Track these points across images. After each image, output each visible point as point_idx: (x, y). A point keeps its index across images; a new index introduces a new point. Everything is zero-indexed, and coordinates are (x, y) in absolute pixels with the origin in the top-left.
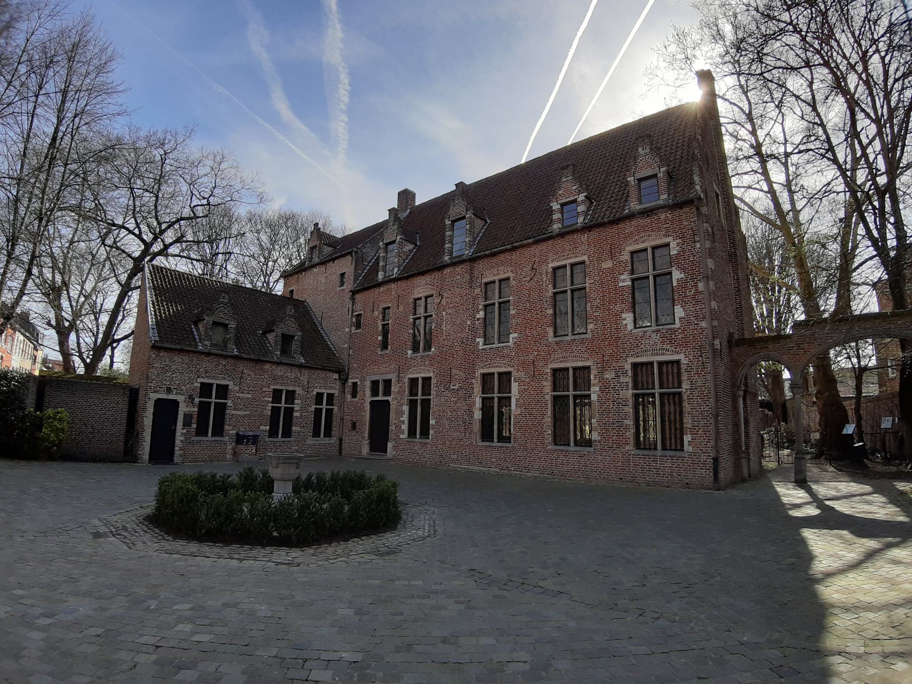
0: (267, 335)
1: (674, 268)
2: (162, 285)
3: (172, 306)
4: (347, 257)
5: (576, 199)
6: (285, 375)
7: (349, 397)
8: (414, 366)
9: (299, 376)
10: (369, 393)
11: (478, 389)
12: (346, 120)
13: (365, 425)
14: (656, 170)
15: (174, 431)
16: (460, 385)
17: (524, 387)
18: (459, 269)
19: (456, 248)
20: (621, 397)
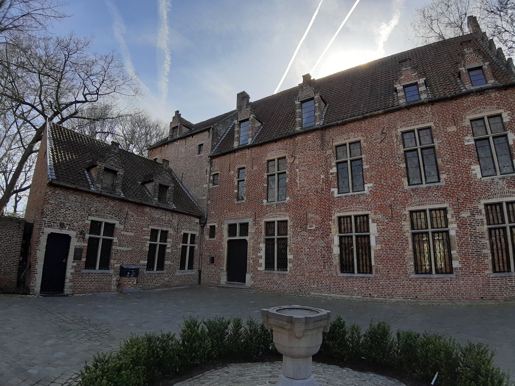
0: (146, 185)
1: (509, 131)
2: (60, 138)
3: (68, 154)
4: (204, 133)
5: (417, 82)
7: (207, 237)
8: (270, 212)
9: (171, 219)
10: (227, 234)
12: (167, 81)
13: (223, 259)
14: (481, 64)
15: (65, 264)
16: (317, 226)
17: (383, 227)
18: (310, 136)
20: (477, 232)
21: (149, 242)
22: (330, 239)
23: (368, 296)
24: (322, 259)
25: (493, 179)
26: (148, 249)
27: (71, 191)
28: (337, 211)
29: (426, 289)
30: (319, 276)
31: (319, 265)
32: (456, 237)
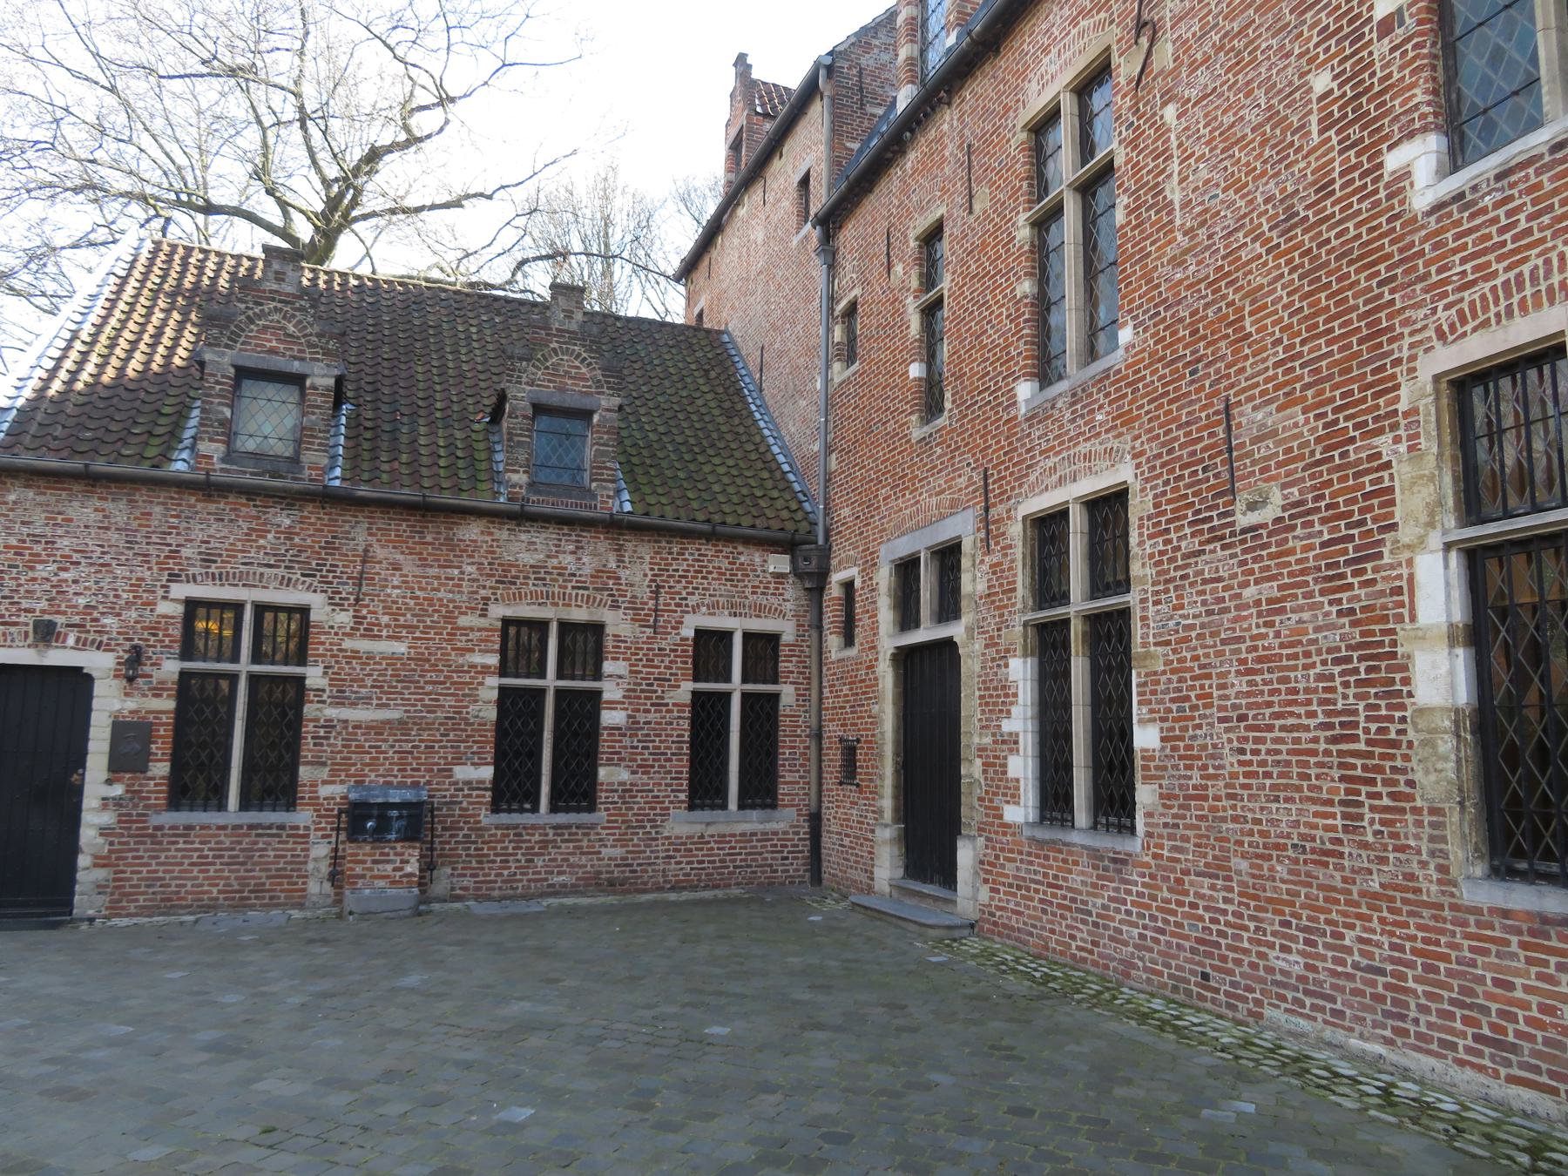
6: (555, 562)
7: (833, 641)
9: (613, 565)
11: (1426, 493)
15: (78, 791)
21: (493, 681)
22: (1386, 586)
24: (1334, 748)
26: (491, 714)
27: (76, 487)
28: (1431, 333)
30: (1320, 887)
31: (1314, 801)
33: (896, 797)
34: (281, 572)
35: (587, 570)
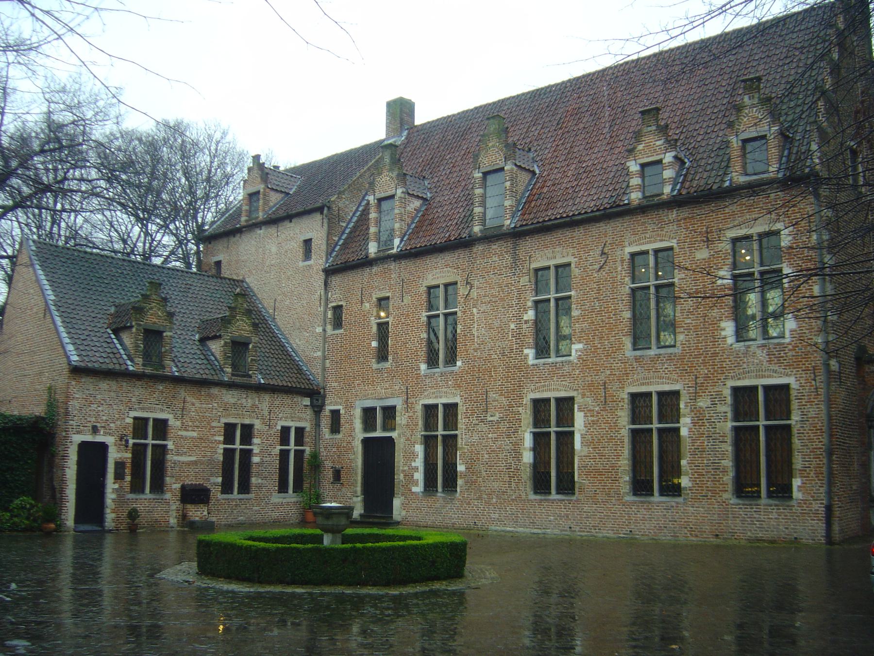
1: (784, 265)
7: (326, 432)
9: (257, 403)
17: (593, 418)
19: (490, 214)
20: (718, 431)
21: (222, 446)
23: (566, 531)
25: (749, 347)
26: (222, 459)
29: (644, 519)
32: (688, 439)
33: (362, 487)
34: (160, 406)
35: (249, 405)
